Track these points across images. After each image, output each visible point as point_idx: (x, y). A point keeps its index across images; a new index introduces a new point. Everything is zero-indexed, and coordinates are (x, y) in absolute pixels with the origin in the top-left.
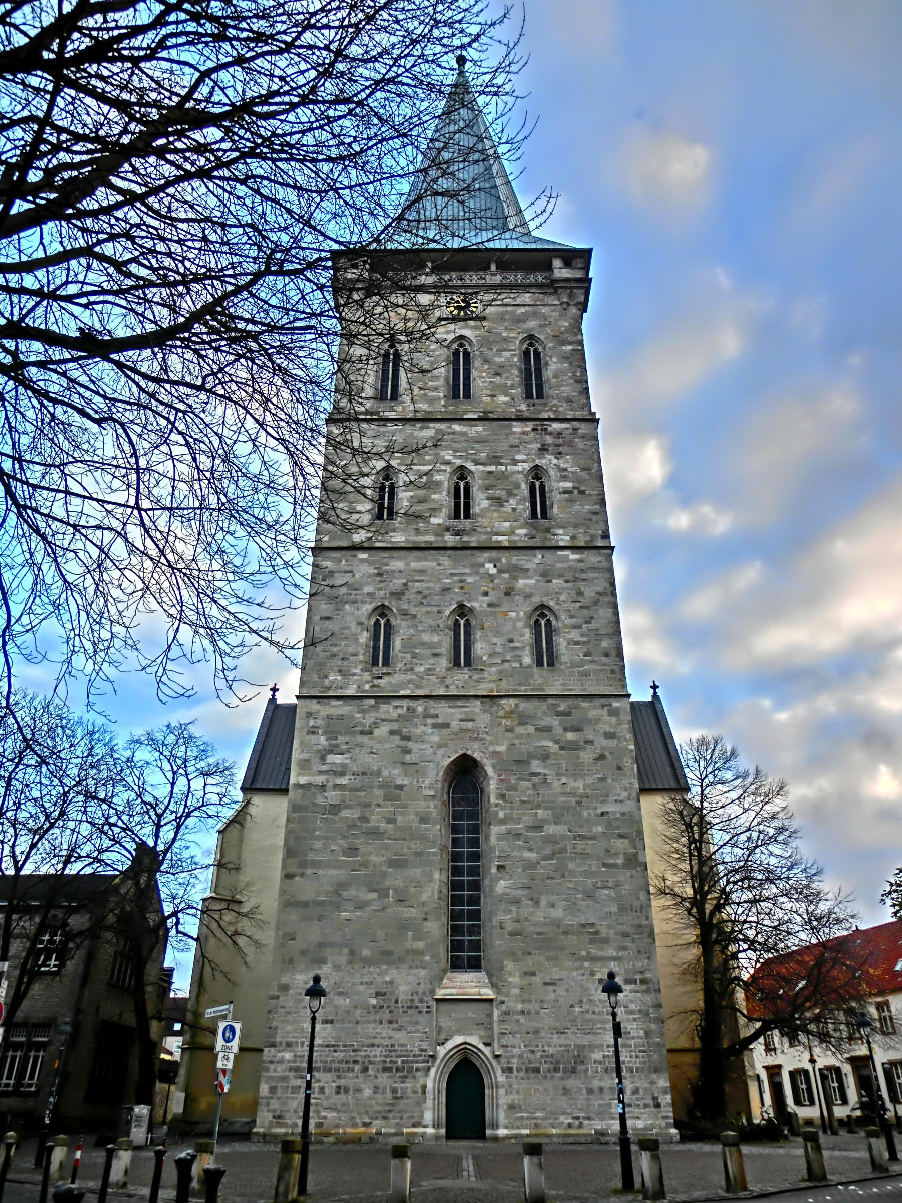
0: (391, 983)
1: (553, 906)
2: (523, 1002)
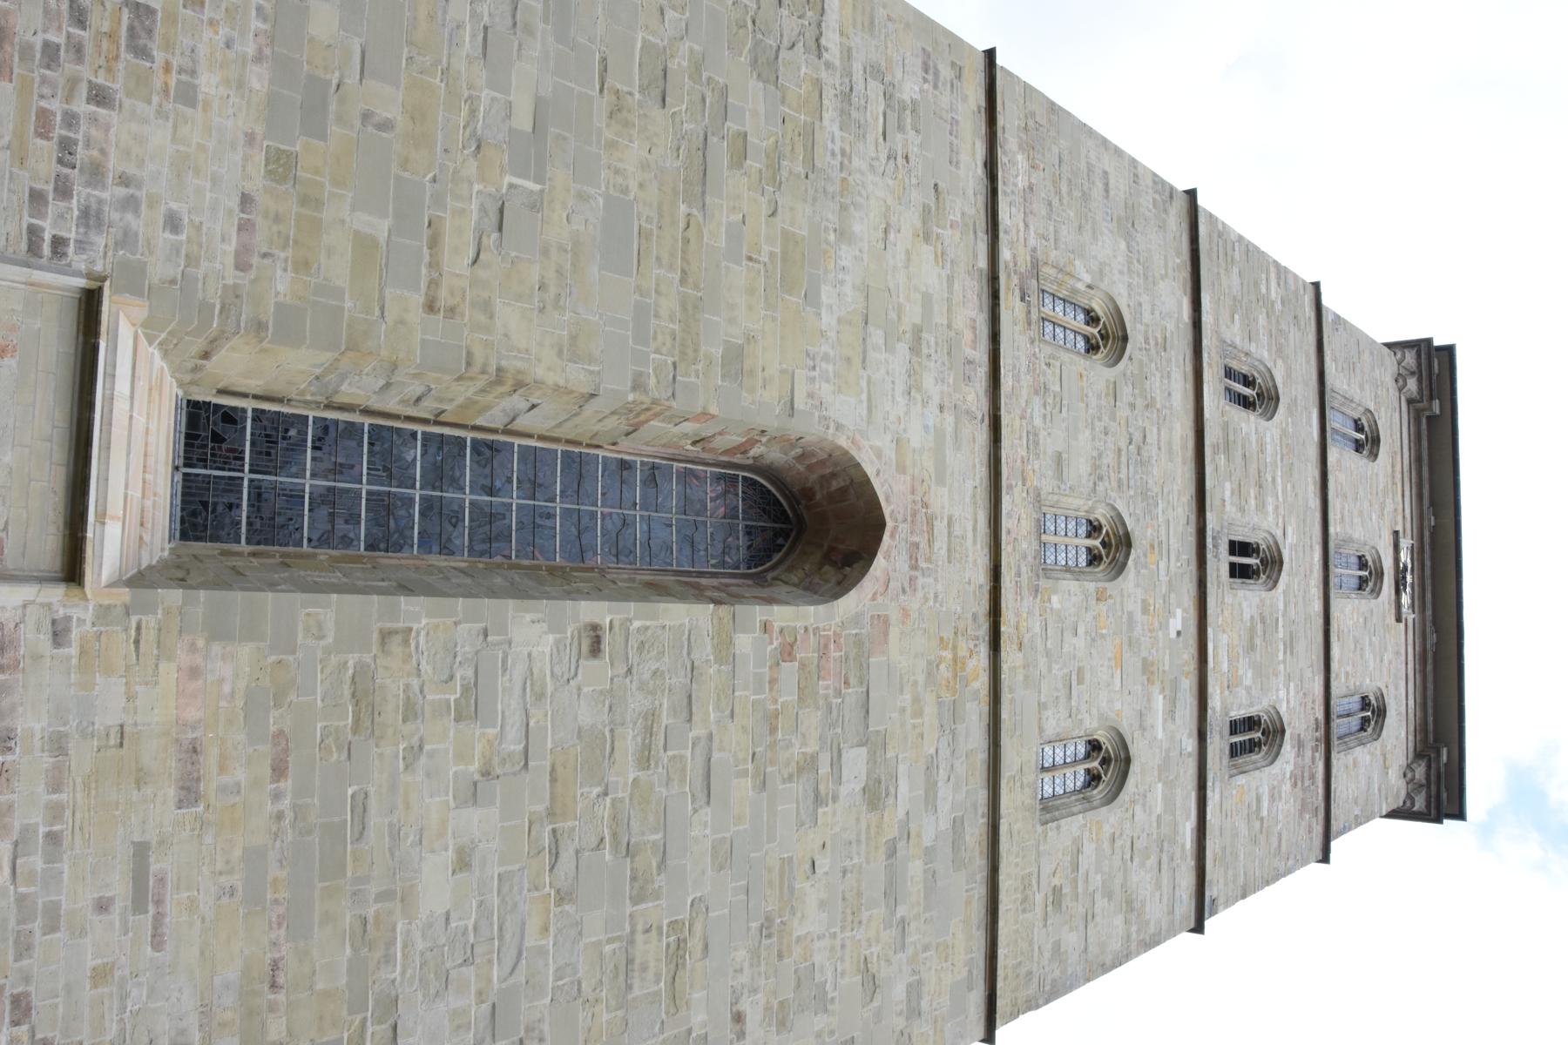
0: (188, 95)
1: (463, 862)
2: (58, 744)
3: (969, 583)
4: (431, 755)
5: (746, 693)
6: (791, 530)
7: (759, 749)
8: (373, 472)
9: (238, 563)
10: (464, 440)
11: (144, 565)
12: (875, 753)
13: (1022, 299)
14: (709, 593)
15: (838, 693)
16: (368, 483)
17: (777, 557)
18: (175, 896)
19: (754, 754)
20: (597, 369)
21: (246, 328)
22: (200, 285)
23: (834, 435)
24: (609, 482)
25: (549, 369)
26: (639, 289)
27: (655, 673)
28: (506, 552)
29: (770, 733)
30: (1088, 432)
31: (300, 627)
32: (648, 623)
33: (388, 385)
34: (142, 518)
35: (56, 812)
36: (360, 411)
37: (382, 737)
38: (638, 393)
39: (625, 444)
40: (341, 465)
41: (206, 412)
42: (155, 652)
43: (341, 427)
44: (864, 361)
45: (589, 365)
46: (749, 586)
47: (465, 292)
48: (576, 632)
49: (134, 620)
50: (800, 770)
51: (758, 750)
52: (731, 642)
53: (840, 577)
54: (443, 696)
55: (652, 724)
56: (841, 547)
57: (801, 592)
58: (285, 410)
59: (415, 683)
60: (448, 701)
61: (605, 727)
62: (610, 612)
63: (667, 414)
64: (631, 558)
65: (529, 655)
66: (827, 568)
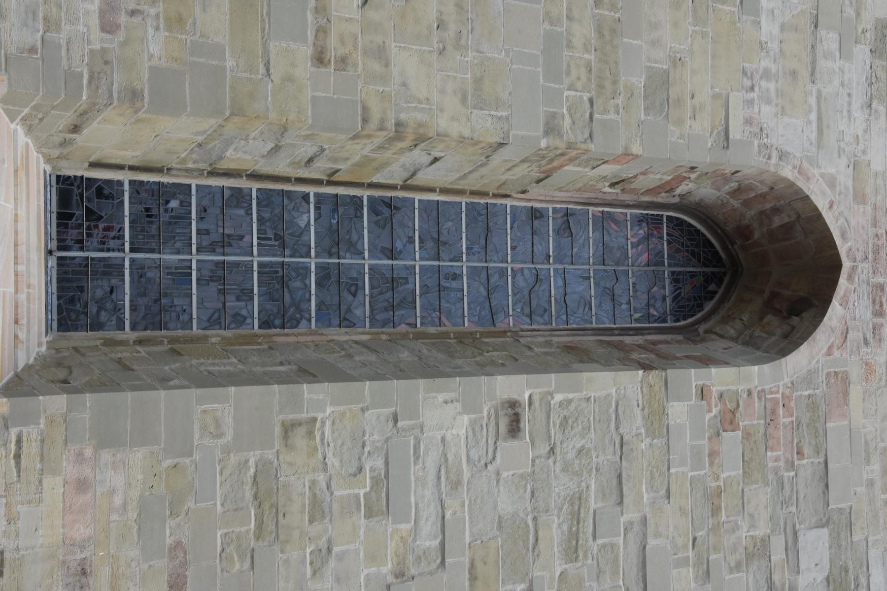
1: (720, 20)
4: (340, 558)
5: (684, 469)
6: (725, 274)
7: (700, 533)
8: (263, 242)
9: (124, 354)
10: (361, 199)
11: (21, 365)
12: (839, 534)
14: (635, 356)
15: (791, 465)
16: (259, 255)
17: (709, 306)
18: (166, 340)
19: (695, 540)
20: (506, 114)
21: (119, 99)
22: (63, 53)
23: (777, 165)
24: (519, 234)
25: (453, 119)
26: (548, 16)
27: (580, 451)
28: (411, 320)
29: (713, 515)
32: (571, 396)
33: (277, 148)
34: (16, 314)
36: (247, 176)
37: (287, 541)
38: (551, 138)
39: (535, 191)
40: (229, 236)
41: (78, 187)
42: (39, 466)
43: (227, 194)
44: (813, 73)
45: (496, 110)
46: (678, 342)
47: (356, 38)
48: (492, 410)
49: (13, 433)
50: (750, 557)
51: (699, 534)
52: (664, 412)
53: (786, 328)
54: (351, 491)
55: (579, 509)
56: (786, 293)
57: (739, 347)
58: (165, 179)
59: (321, 478)
60: (357, 496)
61: (527, 515)
62: (529, 386)
63: (585, 157)
64: (546, 317)
65: (443, 439)
66: (769, 318)
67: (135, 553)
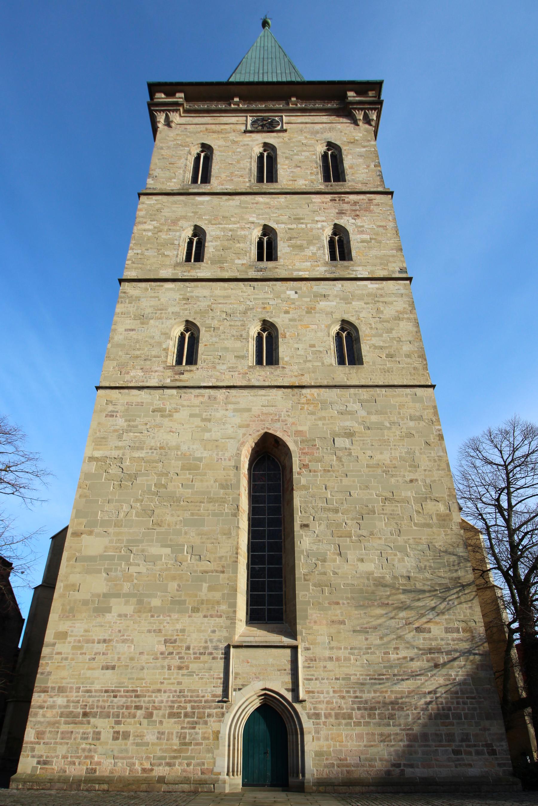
0: (183, 631)
1: (362, 560)
2: (331, 648)
3: (282, 398)
13: (183, 374)
30: (225, 342)
31: (304, 600)
35: (346, 648)
67: (330, 612)
